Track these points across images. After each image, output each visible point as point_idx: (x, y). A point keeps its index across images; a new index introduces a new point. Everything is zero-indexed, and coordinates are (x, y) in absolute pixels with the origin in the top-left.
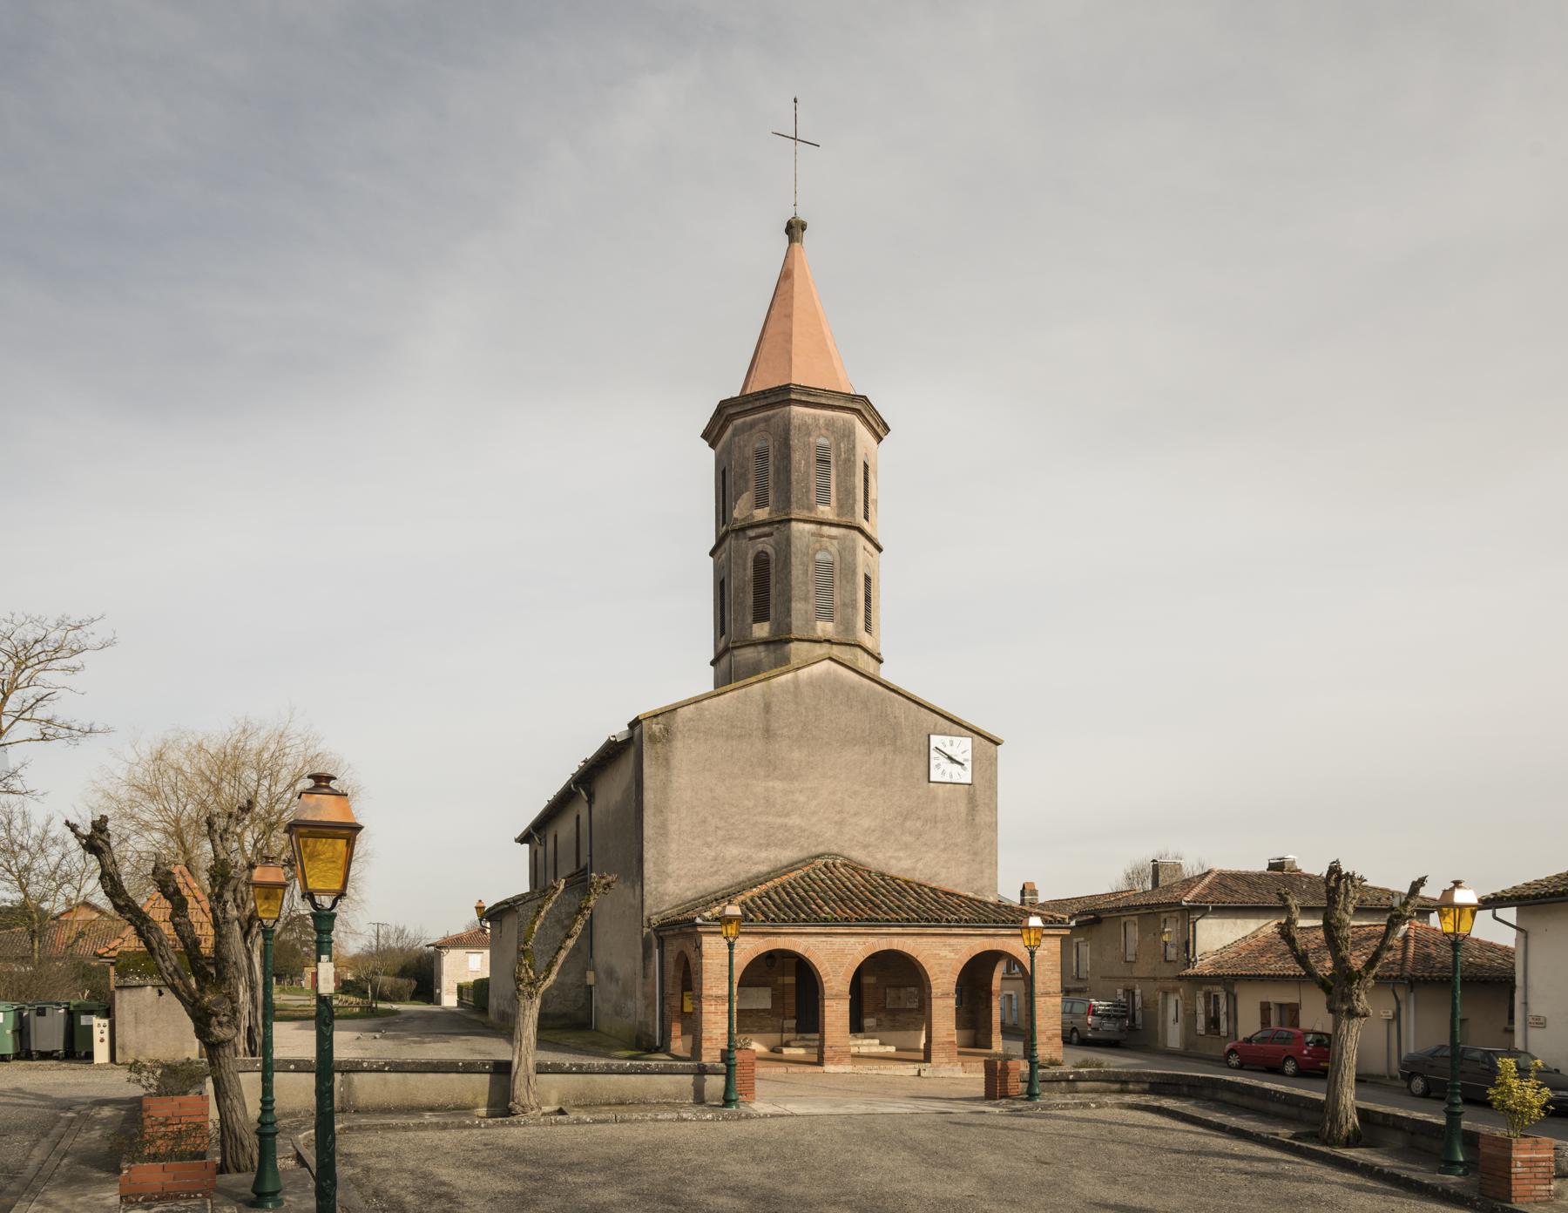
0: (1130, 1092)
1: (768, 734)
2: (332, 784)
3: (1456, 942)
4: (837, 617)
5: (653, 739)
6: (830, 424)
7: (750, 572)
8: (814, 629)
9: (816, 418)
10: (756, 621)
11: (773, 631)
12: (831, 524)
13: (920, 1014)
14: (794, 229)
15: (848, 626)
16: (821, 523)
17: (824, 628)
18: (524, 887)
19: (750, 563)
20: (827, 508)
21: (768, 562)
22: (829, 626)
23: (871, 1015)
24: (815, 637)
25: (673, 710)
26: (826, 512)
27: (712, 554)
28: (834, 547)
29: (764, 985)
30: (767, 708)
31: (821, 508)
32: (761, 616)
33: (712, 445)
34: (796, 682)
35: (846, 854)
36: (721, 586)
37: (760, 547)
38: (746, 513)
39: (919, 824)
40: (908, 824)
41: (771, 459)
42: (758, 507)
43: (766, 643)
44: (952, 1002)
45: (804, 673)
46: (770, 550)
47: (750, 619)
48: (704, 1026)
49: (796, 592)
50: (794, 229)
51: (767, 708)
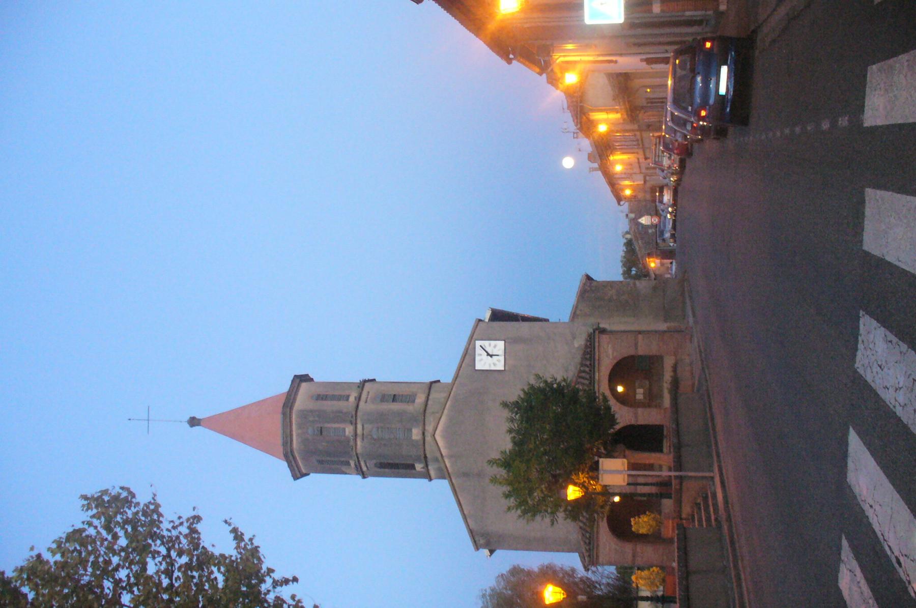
0: (644, 495)
3: (490, 595)
6: (300, 426)
8: (417, 441)
9: (298, 435)
10: (415, 469)
11: (420, 462)
12: (356, 428)
14: (194, 422)
16: (356, 435)
17: (416, 434)
20: (347, 430)
25: (472, 532)
26: (349, 430)
28: (368, 427)
30: (466, 475)
31: (347, 433)
34: (450, 457)
45: (444, 451)
46: (375, 461)
50: (194, 422)
51: (466, 475)
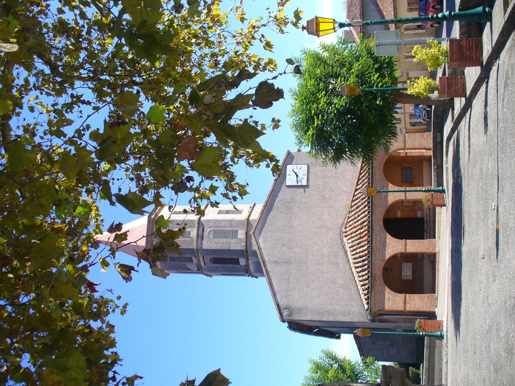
1: (287, 262)
2: (263, 63)
4: (236, 229)
5: (290, 315)
7: (218, 265)
8: (241, 239)
13: (414, 259)
15: (239, 223)
18: (352, 335)
19: (215, 265)
21: (214, 259)
22: (240, 232)
23: (416, 213)
24: (245, 239)
27: (212, 277)
29: (401, 266)
32: (237, 262)
33: (168, 275)
35: (340, 226)
36: (224, 275)
37: (208, 261)
38: (195, 265)
39: (326, 190)
40: (327, 196)
41: (174, 256)
42: (192, 261)
43: (247, 260)
44: (409, 241)
46: (210, 257)
47: (238, 266)
48: (416, 310)
49: (225, 247)
